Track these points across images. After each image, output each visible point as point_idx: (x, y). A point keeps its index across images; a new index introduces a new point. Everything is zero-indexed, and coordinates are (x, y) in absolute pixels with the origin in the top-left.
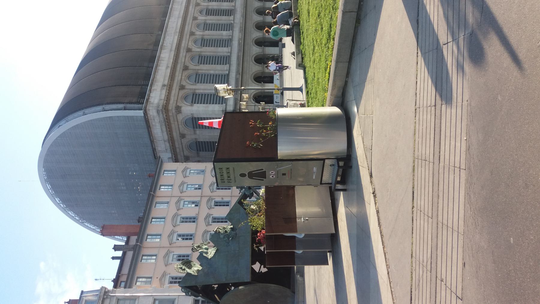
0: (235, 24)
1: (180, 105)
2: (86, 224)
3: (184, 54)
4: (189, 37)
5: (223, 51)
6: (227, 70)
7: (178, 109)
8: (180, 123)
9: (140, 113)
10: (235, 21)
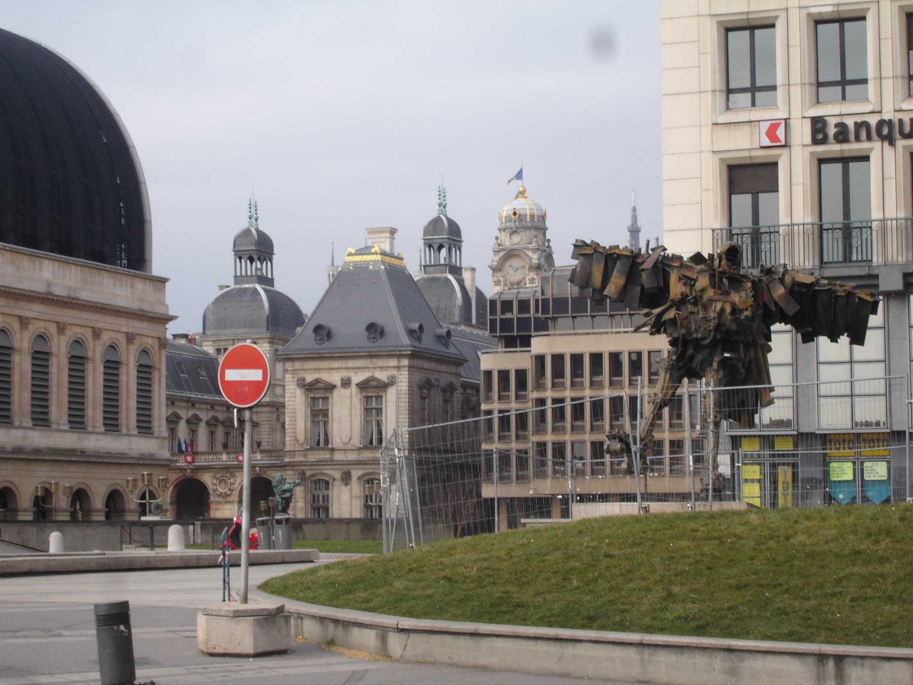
4: (15, 316)
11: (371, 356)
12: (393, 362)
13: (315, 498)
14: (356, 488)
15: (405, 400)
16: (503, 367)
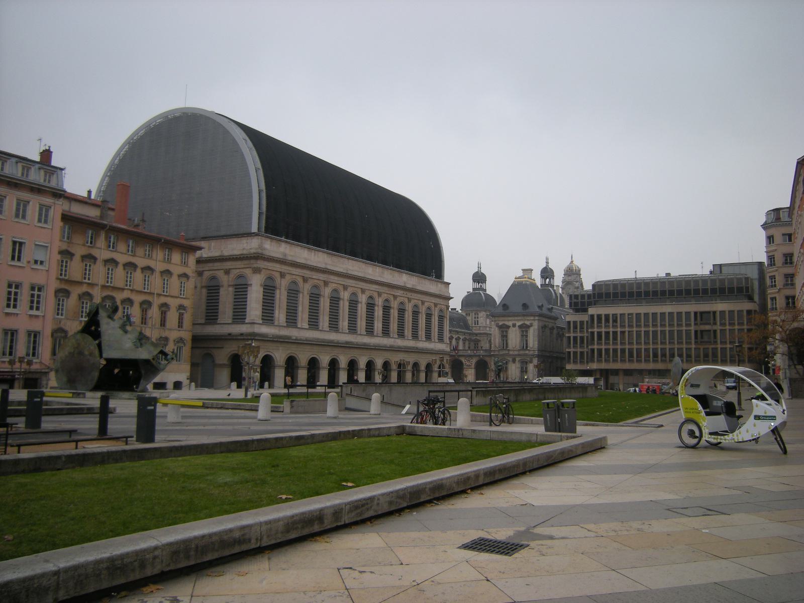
0: (355, 336)
1: (262, 272)
2: (127, 147)
3: (321, 278)
5: (344, 324)
6: (323, 328)
7: (257, 271)
8: (242, 270)
9: (254, 229)
10: (359, 336)
11: (524, 315)
12: (532, 318)
13: (522, 368)
14: (518, 365)
15: (536, 332)
16: (575, 320)
